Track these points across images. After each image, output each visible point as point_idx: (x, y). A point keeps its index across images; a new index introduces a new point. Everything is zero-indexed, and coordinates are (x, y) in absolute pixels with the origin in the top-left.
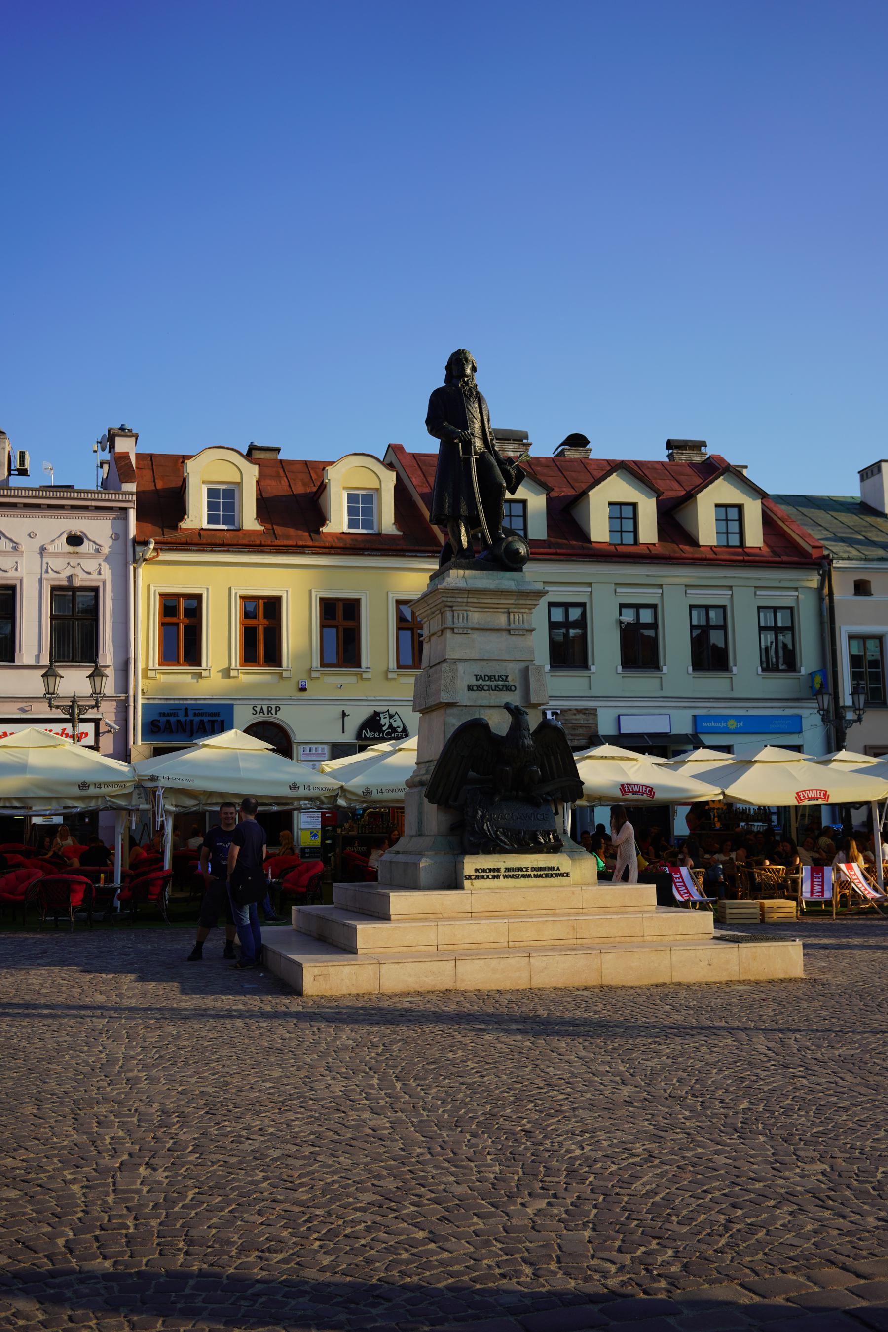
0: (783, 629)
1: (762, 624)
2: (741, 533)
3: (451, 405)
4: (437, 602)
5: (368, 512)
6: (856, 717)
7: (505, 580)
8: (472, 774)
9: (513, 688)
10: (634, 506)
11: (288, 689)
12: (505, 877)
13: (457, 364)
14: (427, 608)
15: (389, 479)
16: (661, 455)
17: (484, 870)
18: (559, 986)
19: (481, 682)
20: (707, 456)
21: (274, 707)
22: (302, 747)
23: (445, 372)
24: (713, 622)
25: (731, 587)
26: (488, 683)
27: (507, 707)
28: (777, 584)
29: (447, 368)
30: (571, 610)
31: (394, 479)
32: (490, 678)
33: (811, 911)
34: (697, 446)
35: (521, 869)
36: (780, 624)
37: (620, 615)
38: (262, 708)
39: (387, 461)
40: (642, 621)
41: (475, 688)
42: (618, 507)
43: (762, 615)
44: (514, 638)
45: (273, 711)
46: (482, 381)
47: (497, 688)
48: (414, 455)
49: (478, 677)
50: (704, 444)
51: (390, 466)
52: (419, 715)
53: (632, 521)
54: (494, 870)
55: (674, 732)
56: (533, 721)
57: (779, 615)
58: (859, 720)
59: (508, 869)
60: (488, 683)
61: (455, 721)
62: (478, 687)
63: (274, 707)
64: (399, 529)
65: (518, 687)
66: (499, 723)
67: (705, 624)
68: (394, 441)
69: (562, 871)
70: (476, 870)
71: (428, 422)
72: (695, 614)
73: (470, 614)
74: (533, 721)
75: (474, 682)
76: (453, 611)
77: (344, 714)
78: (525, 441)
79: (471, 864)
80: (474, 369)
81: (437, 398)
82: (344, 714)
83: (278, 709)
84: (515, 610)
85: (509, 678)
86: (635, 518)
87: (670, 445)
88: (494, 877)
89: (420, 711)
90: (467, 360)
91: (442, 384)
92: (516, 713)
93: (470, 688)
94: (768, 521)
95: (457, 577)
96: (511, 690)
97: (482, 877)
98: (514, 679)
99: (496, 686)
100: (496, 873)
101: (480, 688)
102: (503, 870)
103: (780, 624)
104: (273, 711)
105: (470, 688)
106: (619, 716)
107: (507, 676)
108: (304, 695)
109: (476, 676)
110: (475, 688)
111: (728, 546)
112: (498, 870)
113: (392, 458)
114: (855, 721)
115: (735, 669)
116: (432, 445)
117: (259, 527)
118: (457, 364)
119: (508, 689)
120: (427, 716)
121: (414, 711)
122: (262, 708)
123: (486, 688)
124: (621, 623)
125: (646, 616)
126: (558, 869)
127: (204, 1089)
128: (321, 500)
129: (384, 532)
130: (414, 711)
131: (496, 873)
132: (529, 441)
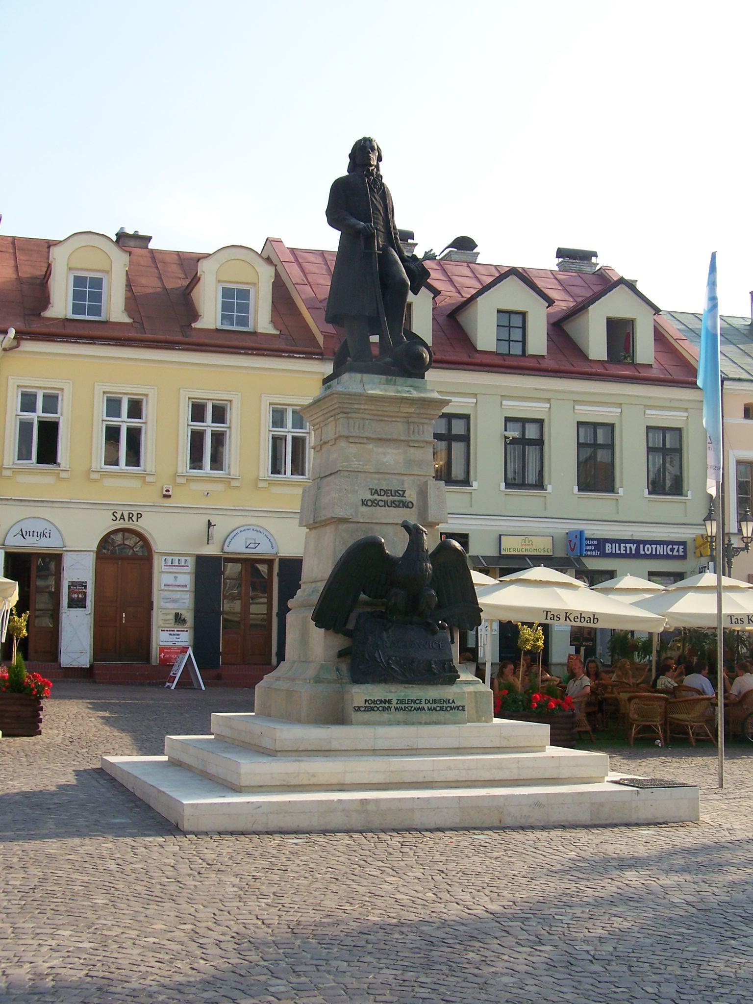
0: (602, 446)
1: (650, 445)
2: (524, 342)
3: (358, 196)
4: (331, 409)
5: (244, 308)
6: (743, 545)
7: (403, 389)
8: (363, 597)
9: (410, 505)
10: (523, 314)
11: (149, 496)
12: (396, 709)
13: (363, 154)
14: (320, 414)
15: (266, 275)
16: (552, 263)
17: (374, 702)
18: (119, 779)
19: (376, 496)
20: (598, 267)
21: (135, 514)
22: (164, 558)
23: (348, 160)
24: (600, 440)
25: (621, 404)
26: (385, 498)
27: (406, 526)
28: (667, 404)
29: (350, 156)
30: (454, 422)
31: (273, 275)
32: (386, 493)
33: (642, 739)
34: (586, 256)
35: (413, 701)
36: (668, 446)
37: (506, 430)
38: (122, 514)
39: (265, 256)
40: (453, 432)
41: (369, 503)
42: (507, 315)
43: (650, 435)
44: (412, 450)
45: (134, 518)
46: (390, 173)
47: (394, 504)
48: (292, 251)
49: (374, 492)
50: (595, 254)
51: (269, 260)
52: (305, 530)
53: (520, 330)
54: (385, 701)
55: (555, 556)
56: (430, 543)
57: (668, 436)
58: (746, 548)
59: (401, 701)
60: (385, 498)
61: (348, 538)
62: (373, 502)
63: (135, 514)
64: (276, 328)
65: (415, 503)
66: (396, 545)
67: (592, 442)
68: (379, 141)
69: (458, 704)
70: (366, 701)
71: (328, 213)
72: (582, 430)
73: (425, 426)
74: (430, 543)
75: (368, 496)
76: (408, 423)
77: (210, 524)
78: (410, 241)
79: (360, 694)
80: (380, 159)
81: (340, 190)
82: (210, 524)
83: (139, 516)
84: (417, 420)
85: (406, 494)
86: (524, 328)
87: (561, 253)
88: (384, 709)
89: (307, 526)
90: (373, 149)
91: (344, 173)
92: (414, 533)
93: (364, 503)
94: (660, 337)
95: (351, 382)
96: (408, 507)
97: (372, 709)
98: (411, 495)
99: (393, 502)
100: (387, 705)
101: (375, 503)
102: (394, 702)
103: (668, 446)
104: (134, 518)
105: (364, 503)
106: (500, 536)
107: (404, 492)
108: (167, 502)
109: (371, 489)
110: (369, 503)
111: (509, 355)
112: (390, 701)
113: (269, 253)
114: (742, 549)
115: (621, 491)
116: (330, 240)
117: (271, 330)
118: (363, 154)
119: (407, 505)
120: (314, 532)
121: (301, 525)
122: (122, 514)
123: (381, 503)
124: (506, 438)
125: (531, 432)
126: (453, 701)
127: (80, 945)
128: (195, 294)
129: (259, 331)
130: (301, 525)
131: (387, 705)
132: (415, 241)
